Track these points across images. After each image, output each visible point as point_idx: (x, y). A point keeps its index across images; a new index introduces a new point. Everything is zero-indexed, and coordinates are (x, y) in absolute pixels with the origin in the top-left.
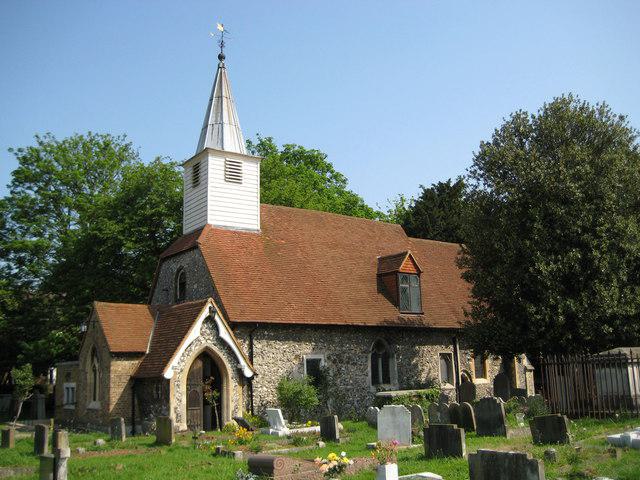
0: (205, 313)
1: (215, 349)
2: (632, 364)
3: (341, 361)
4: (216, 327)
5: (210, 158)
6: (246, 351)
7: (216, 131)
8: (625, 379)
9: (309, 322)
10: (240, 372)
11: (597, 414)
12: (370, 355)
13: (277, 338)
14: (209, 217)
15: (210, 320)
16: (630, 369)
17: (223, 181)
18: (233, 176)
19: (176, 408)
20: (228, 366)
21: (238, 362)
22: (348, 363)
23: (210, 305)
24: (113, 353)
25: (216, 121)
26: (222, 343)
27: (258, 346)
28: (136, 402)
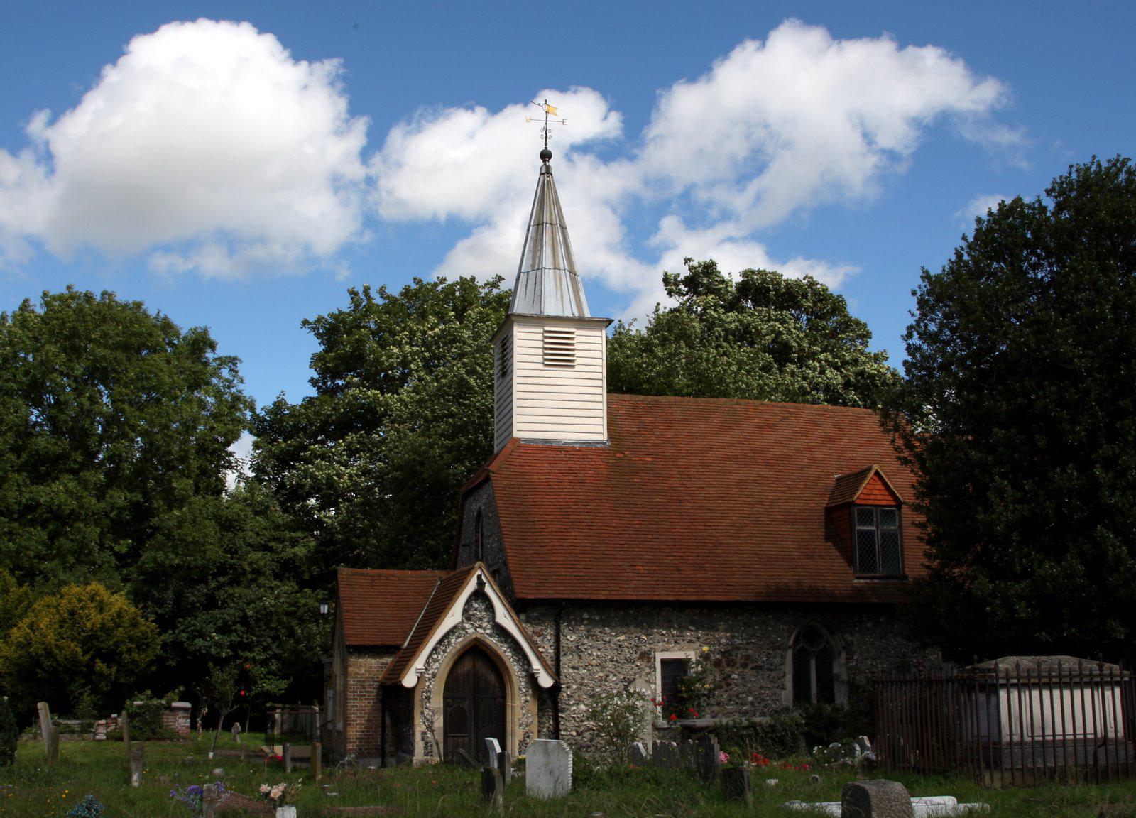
0: (471, 586)
1: (493, 641)
2: (1008, 686)
3: (731, 663)
4: (490, 608)
5: (516, 329)
6: (548, 649)
7: (531, 282)
8: (993, 711)
9: (663, 598)
10: (532, 679)
11: (924, 769)
12: (789, 654)
13: (605, 623)
14: (516, 427)
15: (479, 595)
16: (1003, 694)
17: (541, 366)
18: (559, 356)
19: (424, 733)
20: (515, 669)
21: (529, 664)
22: (745, 666)
23: (479, 572)
24: (349, 647)
25: (533, 266)
26: (501, 631)
27: (570, 638)
28: (388, 721)
